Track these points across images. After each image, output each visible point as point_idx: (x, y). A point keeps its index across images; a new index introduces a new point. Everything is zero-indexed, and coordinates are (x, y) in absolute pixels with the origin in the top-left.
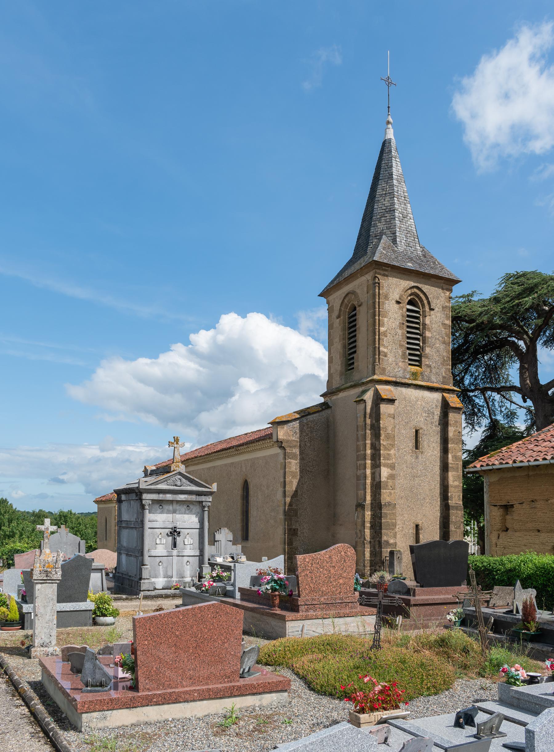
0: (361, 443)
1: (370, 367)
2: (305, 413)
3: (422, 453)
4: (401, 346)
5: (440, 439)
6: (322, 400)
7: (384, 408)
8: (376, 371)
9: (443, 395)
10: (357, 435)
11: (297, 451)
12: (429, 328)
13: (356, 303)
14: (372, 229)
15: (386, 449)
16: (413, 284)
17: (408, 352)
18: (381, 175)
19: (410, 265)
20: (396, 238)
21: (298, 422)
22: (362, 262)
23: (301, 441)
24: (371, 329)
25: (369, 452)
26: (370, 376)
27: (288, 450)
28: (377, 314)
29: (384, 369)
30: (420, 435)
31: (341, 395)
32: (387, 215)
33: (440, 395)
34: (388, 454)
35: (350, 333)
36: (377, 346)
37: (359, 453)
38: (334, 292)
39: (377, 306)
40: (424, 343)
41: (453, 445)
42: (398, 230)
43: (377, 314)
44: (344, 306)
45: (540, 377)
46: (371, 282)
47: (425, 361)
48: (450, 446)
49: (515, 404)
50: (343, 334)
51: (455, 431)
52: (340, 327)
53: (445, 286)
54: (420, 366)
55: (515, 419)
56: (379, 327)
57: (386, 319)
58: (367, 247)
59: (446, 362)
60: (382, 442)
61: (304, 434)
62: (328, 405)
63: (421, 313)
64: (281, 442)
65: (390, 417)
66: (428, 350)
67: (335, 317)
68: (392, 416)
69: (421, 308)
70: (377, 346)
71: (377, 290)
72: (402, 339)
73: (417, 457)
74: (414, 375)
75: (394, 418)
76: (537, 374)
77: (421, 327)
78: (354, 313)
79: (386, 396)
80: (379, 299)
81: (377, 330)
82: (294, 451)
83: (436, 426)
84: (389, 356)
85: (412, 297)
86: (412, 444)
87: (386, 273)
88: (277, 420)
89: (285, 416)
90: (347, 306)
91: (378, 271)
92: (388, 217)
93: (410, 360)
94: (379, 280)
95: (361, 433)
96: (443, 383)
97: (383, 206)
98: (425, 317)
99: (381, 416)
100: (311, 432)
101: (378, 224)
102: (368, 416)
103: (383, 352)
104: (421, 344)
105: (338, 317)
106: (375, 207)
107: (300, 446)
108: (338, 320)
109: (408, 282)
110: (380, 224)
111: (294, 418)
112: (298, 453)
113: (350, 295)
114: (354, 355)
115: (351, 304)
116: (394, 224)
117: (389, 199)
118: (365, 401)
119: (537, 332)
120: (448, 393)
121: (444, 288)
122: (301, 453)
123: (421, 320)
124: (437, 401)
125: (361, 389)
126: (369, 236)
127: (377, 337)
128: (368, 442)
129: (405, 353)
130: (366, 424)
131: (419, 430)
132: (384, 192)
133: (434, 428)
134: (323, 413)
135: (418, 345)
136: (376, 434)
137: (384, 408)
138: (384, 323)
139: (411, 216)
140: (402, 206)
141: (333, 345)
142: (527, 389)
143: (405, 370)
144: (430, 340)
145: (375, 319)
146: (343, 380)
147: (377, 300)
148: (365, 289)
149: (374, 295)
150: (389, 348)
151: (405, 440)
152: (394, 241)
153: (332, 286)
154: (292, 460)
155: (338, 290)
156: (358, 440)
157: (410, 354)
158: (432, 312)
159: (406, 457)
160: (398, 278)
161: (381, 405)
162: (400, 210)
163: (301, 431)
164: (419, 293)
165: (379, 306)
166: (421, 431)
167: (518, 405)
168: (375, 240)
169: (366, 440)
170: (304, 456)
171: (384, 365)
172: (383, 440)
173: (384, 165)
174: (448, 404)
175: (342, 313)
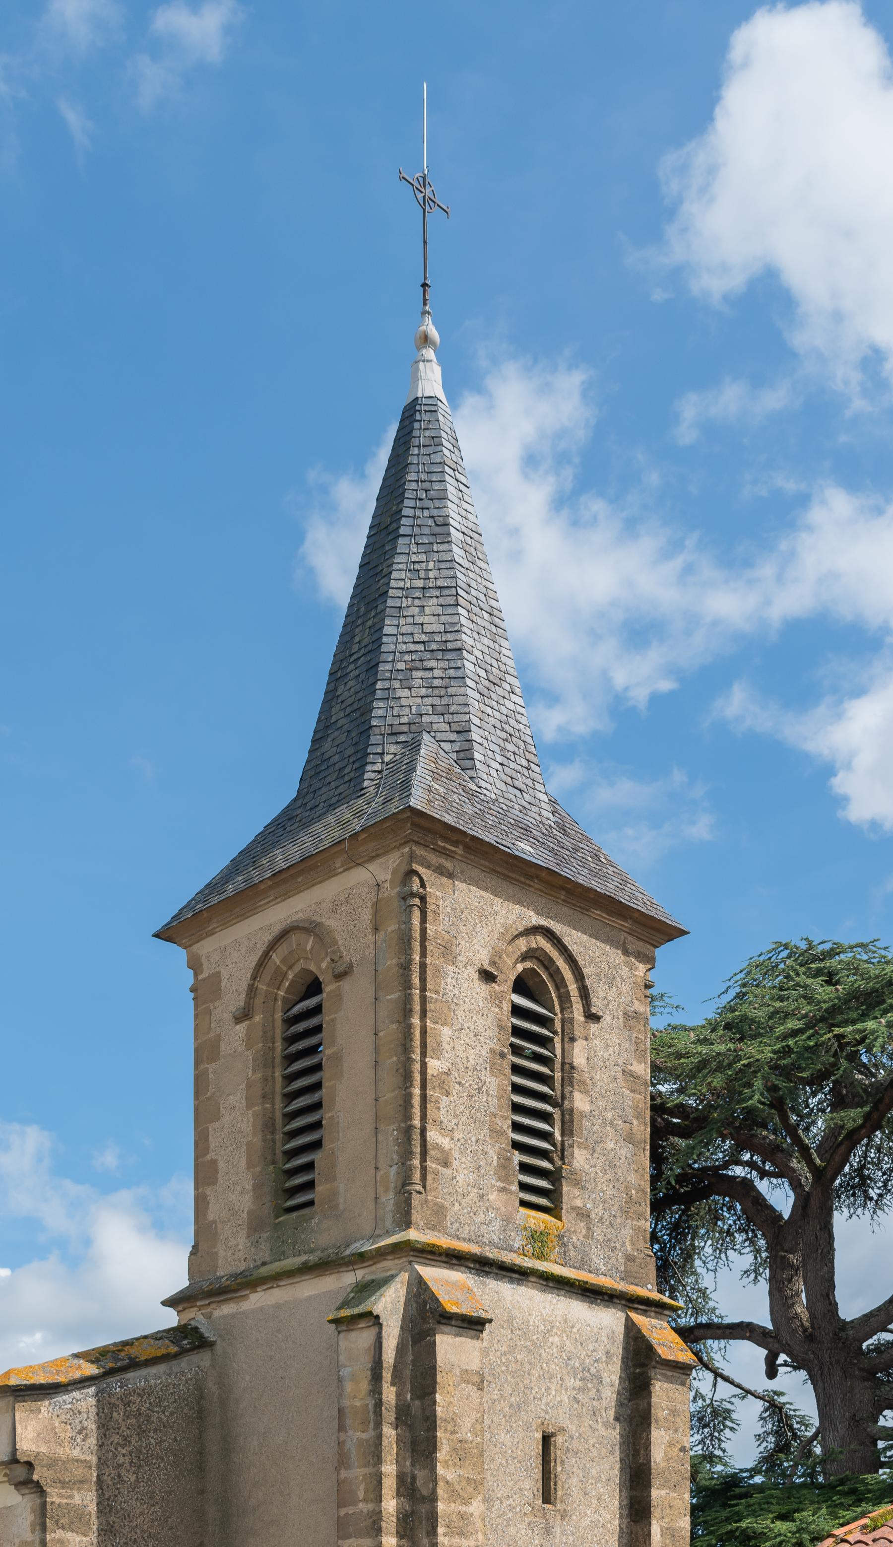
0: (358, 1473)
1: (389, 1199)
2: (117, 1362)
3: (564, 1515)
4: (496, 1132)
5: (621, 1469)
6: (171, 1319)
7: (449, 1347)
8: (415, 1216)
9: (628, 1317)
10: (340, 1444)
11: (87, 1500)
12: (582, 1082)
13: (321, 968)
14: (379, 709)
15: (455, 1496)
16: (536, 920)
17: (518, 1157)
18: (404, 521)
19: (524, 848)
20: (470, 749)
21: (92, 1390)
22: (348, 818)
23: (102, 1463)
24: (391, 1061)
25: (390, 1505)
26: (388, 1233)
27: (54, 1496)
28: (417, 1007)
29: (440, 1211)
30: (557, 1453)
31: (257, 1300)
32: (432, 664)
33: (621, 1316)
34: (463, 1516)
35: (290, 1078)
36: (417, 1122)
37: (350, 1510)
38: (225, 925)
39: (416, 981)
40: (567, 1129)
41: (663, 1492)
42: (476, 721)
43: (417, 1007)
44: (267, 975)
45: (840, 1295)
46: (390, 891)
47: (571, 1196)
48: (655, 1493)
49: (732, 1383)
50: (265, 1080)
51: (670, 1444)
52: (250, 1055)
53: (635, 945)
54: (554, 1211)
55: (727, 1431)
56: (423, 1054)
57: (446, 1031)
58: (361, 769)
59: (636, 1208)
60: (440, 1470)
61: (116, 1438)
62: (201, 1336)
63: (558, 1026)
64: (30, 1465)
65: (467, 1382)
66: (579, 1158)
67: (228, 1017)
68: (476, 1379)
69: (557, 1008)
70: (417, 1122)
71: (416, 922)
72: (500, 1107)
73: (548, 1532)
74: (536, 1238)
75: (480, 1389)
76: (833, 1287)
77: (558, 1075)
78: (311, 1002)
79: (456, 1304)
80: (423, 954)
81: (417, 1067)
82: (77, 1500)
83: (606, 1424)
84: (455, 1164)
85: (528, 964)
86: (531, 1483)
87: (448, 865)
88: (13, 1382)
89: (43, 1367)
90: (279, 977)
91: (420, 851)
92: (437, 673)
93: (524, 1187)
94: (423, 885)
95: (356, 1436)
96: (626, 1276)
97: (418, 629)
98: (573, 1040)
99: (439, 1378)
100: (142, 1433)
101: (399, 693)
102: (387, 1375)
103: (438, 1147)
104: (558, 1136)
105: (244, 1015)
106: (387, 630)
107: (100, 1481)
108: (241, 1028)
109: (518, 908)
110: (407, 693)
111: (77, 1375)
112: (93, 1508)
113: (294, 937)
114: (316, 1156)
115: (297, 969)
116: (461, 700)
117: (439, 610)
118: (375, 1320)
119: (843, 1148)
120: (644, 1313)
121: (630, 948)
122: (105, 1507)
123: (558, 1052)
124: (611, 1337)
125: (349, 1278)
126: (366, 731)
127: (416, 1091)
128: (389, 1469)
129: (509, 1160)
130: (379, 1404)
131: (553, 1435)
132: (420, 583)
133: (602, 1431)
134: (183, 1363)
135: (545, 1136)
136: (421, 1442)
137: (449, 1347)
138: (439, 1044)
139: (515, 682)
140: (485, 641)
141: (216, 1116)
142: (794, 1331)
143: (507, 1220)
144: (585, 1123)
145: (410, 1026)
146: (265, 1246)
147: (417, 958)
148: (366, 916)
149: (405, 940)
150: (458, 1135)
151: (511, 1469)
152: (465, 756)
153: (215, 900)
154: (69, 1535)
155: (243, 917)
156: (342, 1461)
157: (525, 1168)
158: (593, 1027)
159: (512, 1530)
160: (485, 889)
161: (439, 1338)
162: (479, 655)
163: (105, 1425)
164: (554, 953)
165: (423, 980)
166: (559, 1439)
167: (738, 1386)
168: (393, 749)
169: (379, 1460)
170: (112, 1519)
171: (438, 1193)
172: (446, 1464)
173: (414, 486)
174: (650, 1348)
175: (259, 1001)
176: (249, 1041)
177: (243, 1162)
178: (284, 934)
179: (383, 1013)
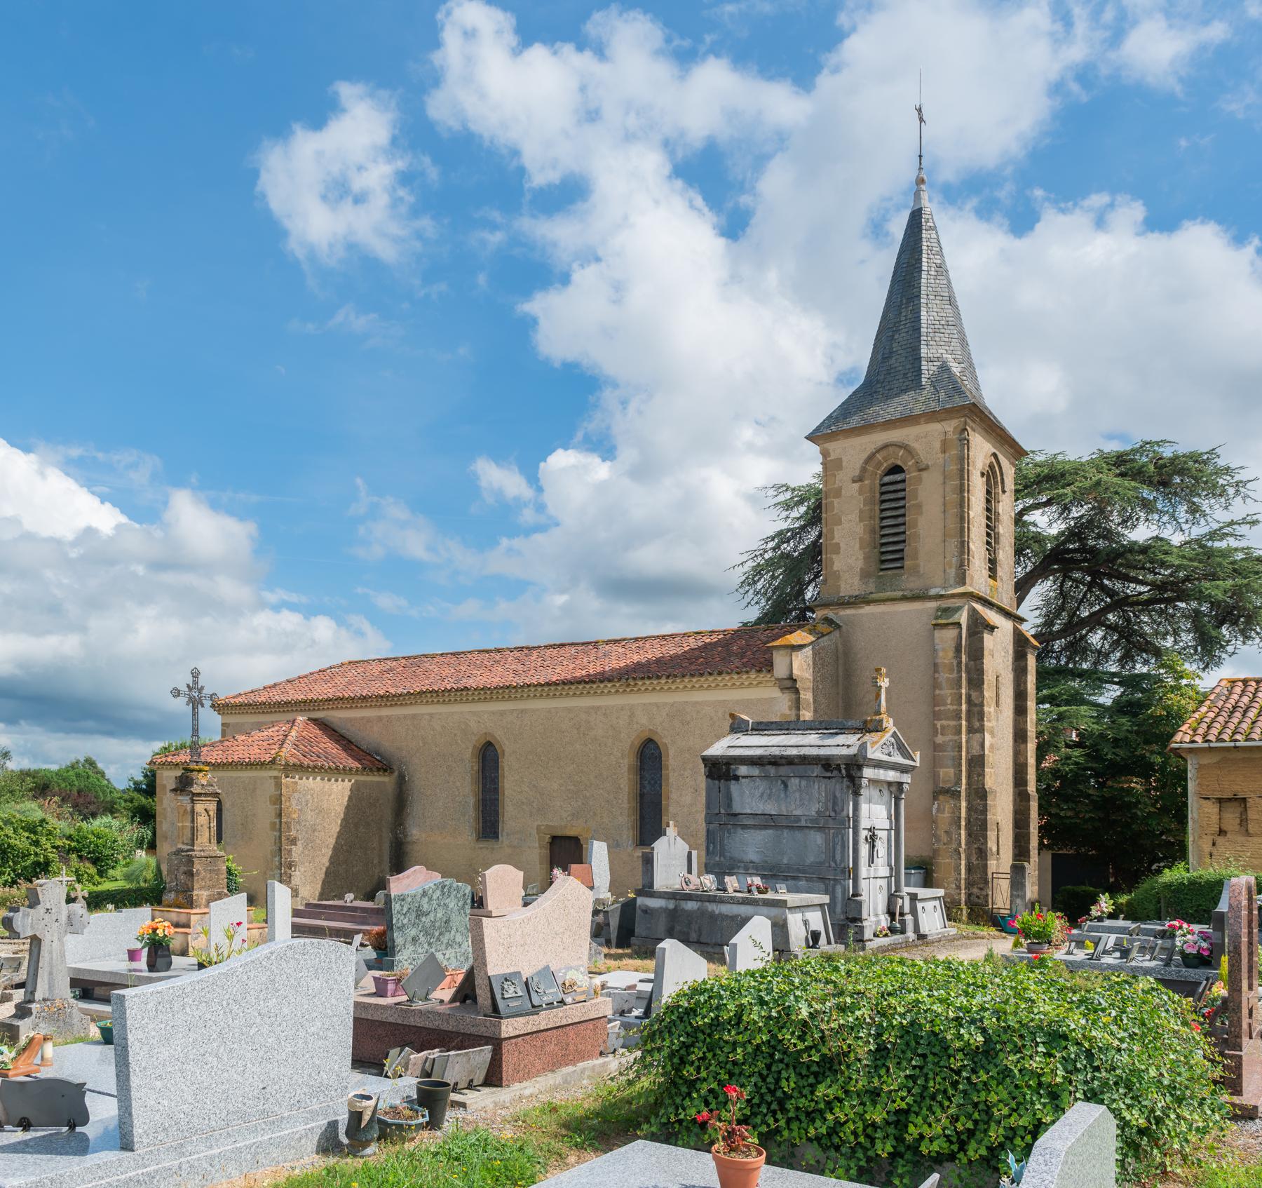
1: (952, 572)
24: (954, 511)
46: (952, 436)
105: (859, 479)
108: (856, 486)
118: (959, 625)
128: (963, 691)
156: (936, 685)
176: (861, 492)
177: (857, 546)
178: (885, 446)
179: (948, 489)
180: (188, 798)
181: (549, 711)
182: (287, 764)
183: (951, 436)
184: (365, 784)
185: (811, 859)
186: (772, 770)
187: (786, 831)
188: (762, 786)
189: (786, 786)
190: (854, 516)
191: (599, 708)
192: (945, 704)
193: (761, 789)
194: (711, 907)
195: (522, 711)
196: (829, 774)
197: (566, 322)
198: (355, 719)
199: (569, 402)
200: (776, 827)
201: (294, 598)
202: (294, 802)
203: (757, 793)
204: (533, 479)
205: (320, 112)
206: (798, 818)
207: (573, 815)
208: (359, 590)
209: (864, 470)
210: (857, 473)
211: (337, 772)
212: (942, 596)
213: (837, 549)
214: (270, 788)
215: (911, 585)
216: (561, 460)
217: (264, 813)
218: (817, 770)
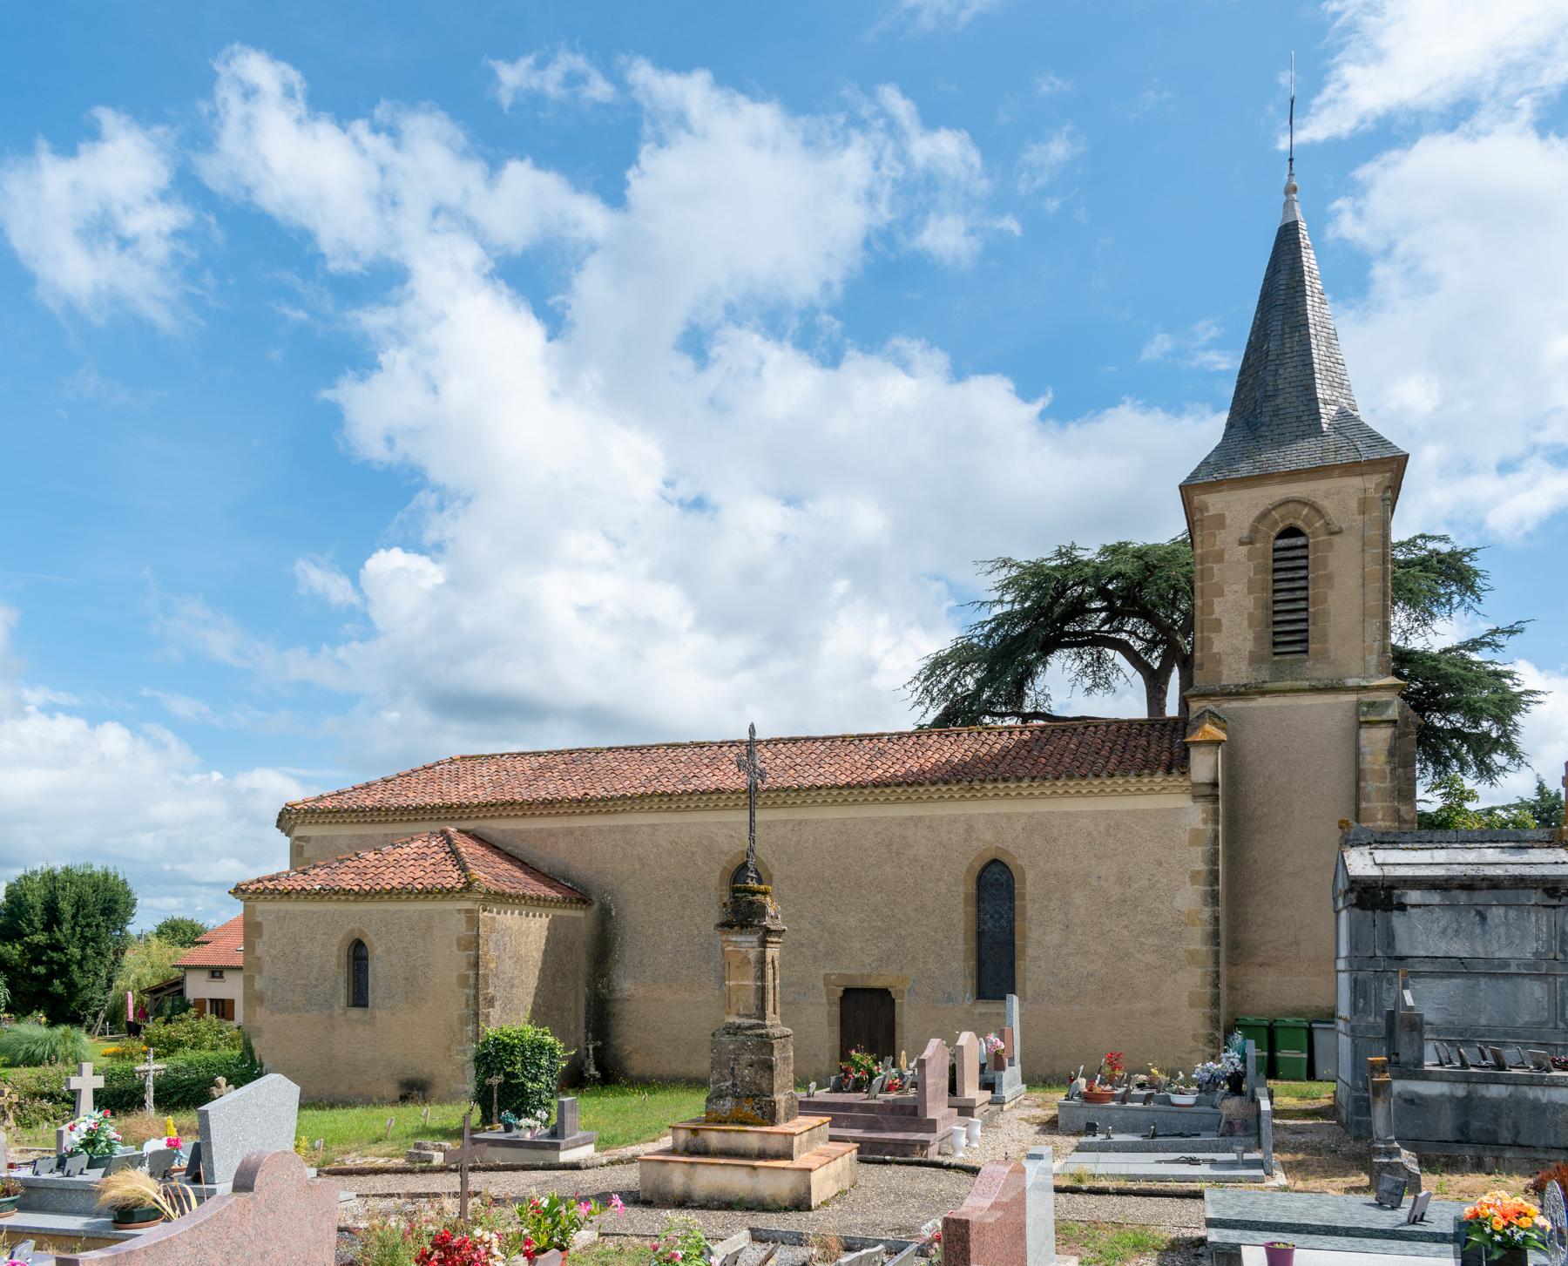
105: (1249, 541)
108: (1244, 549)
176: (1250, 556)
177: (1246, 623)
178: (1286, 502)
179: (1368, 558)
180: (754, 939)
181: (844, 823)
182: (488, 892)
183: (1372, 493)
184: (561, 917)
185: (1524, 1018)
186: (1462, 897)
187: (1483, 981)
188: (1444, 918)
189: (1483, 918)
190: (1242, 587)
191: (920, 819)
192: (1375, 820)
193: (1443, 923)
194: (1532, 1093)
195: (800, 823)
196: (1555, 902)
197: (377, 410)
198: (528, 831)
199: (390, 499)
200: (1468, 974)
201: (63, 698)
202: (491, 944)
203: (1436, 928)
204: (355, 580)
205: (73, 136)
206: (1505, 963)
207: (881, 960)
208: (145, 692)
209: (1254, 530)
210: (1245, 533)
211: (538, 902)
212: (1365, 688)
213: (1217, 626)
214: (460, 927)
215: (1318, 674)
216: (387, 563)
217: (447, 963)
218: (1536, 897)
